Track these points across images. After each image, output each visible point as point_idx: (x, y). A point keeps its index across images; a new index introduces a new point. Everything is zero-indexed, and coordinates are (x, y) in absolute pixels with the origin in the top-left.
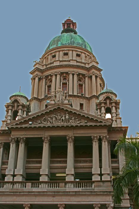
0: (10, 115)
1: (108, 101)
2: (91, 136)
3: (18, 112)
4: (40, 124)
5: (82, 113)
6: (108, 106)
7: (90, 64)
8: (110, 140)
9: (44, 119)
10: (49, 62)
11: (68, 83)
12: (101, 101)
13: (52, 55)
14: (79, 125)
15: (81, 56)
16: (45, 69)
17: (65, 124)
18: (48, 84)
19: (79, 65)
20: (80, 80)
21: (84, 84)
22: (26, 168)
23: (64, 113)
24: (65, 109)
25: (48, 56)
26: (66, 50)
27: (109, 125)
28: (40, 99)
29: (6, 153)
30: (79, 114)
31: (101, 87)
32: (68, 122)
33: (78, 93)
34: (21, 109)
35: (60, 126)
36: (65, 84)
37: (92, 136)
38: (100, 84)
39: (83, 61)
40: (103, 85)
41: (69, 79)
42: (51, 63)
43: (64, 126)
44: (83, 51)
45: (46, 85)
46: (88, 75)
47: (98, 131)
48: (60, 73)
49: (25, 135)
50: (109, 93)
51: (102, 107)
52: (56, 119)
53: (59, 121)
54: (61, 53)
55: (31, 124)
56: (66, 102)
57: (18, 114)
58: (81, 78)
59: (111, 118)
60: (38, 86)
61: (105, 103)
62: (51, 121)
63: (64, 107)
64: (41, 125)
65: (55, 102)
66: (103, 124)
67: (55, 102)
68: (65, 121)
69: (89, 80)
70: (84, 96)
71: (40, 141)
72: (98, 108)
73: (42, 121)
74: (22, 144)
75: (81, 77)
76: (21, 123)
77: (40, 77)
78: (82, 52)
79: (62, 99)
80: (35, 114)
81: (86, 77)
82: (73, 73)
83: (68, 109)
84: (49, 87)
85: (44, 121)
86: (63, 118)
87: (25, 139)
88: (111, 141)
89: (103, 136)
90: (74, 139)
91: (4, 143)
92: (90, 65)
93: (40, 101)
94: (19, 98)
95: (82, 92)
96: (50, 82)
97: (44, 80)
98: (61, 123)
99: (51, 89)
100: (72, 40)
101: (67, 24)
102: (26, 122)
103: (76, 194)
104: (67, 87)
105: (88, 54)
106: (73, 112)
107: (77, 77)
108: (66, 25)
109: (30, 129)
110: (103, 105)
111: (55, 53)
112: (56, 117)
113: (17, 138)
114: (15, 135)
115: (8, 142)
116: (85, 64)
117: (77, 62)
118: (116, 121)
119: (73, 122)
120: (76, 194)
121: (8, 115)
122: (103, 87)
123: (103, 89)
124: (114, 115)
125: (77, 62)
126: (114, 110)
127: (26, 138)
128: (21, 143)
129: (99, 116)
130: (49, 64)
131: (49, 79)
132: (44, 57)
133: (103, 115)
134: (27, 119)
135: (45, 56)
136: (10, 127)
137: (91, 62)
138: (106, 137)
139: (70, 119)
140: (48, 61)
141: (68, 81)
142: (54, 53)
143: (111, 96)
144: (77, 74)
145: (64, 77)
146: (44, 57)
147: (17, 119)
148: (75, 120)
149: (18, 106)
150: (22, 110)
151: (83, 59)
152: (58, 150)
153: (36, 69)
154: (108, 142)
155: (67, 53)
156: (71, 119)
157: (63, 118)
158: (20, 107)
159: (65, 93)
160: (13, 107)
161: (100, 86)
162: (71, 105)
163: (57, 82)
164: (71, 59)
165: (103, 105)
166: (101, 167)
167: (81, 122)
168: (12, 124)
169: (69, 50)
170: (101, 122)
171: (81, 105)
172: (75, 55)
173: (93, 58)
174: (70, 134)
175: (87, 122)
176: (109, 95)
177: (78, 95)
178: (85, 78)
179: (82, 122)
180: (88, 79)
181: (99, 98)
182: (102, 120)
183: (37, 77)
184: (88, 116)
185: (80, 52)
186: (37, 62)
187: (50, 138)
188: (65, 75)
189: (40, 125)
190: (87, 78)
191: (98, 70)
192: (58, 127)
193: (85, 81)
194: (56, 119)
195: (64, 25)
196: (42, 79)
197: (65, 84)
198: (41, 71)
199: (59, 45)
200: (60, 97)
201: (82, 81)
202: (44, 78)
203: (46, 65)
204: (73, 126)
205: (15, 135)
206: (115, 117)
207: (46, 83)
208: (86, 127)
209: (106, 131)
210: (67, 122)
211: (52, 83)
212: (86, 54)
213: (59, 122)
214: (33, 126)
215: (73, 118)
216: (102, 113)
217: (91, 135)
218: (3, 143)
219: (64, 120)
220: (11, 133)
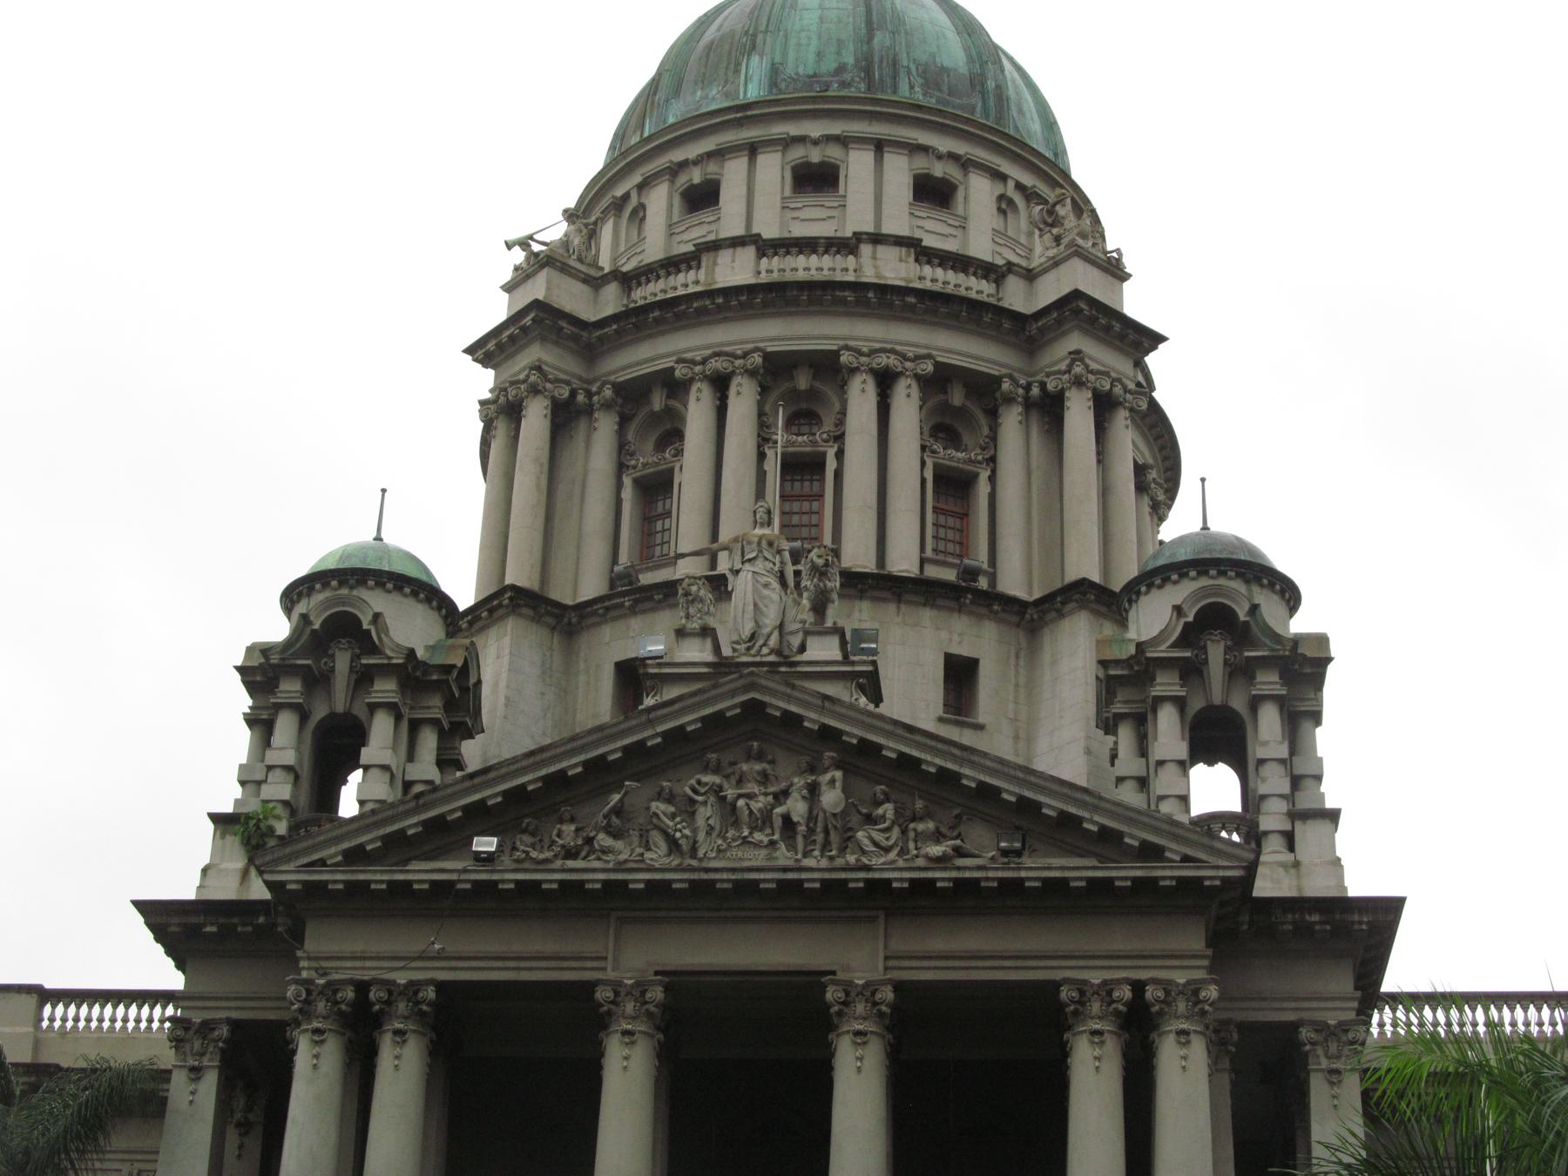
0: (289, 757)
1: (1216, 653)
2: (1056, 985)
3: (358, 735)
4: (571, 854)
5: (973, 765)
6: (1217, 699)
7: (1049, 278)
8: (1228, 1022)
9: (618, 811)
10: (654, 247)
11: (831, 453)
12: (1154, 642)
13: (682, 180)
15: (960, 194)
16: (615, 318)
17: (816, 866)
18: (646, 458)
19: (937, 287)
20: (942, 428)
21: (984, 475)
23: (804, 760)
24: (813, 718)
25: (641, 187)
26: (816, 142)
27: (1224, 879)
28: (564, 607)
29: (238, 1116)
30: (941, 769)
31: (1146, 500)
32: (843, 850)
33: (929, 553)
34: (392, 708)
35: (812, 880)
36: (803, 468)
37: (1067, 981)
38: (1140, 470)
39: (981, 247)
40: (1160, 470)
41: (841, 422)
42: (672, 265)
43: (800, 882)
44: (981, 154)
45: (621, 468)
46: (1028, 388)
47: (1119, 937)
48: (757, 359)
49: (439, 956)
50: (1222, 573)
51: (1159, 701)
52: (729, 811)
53: (758, 836)
54: (772, 170)
55: (488, 859)
56: (824, 650)
57: (366, 755)
58: (961, 412)
59: (1237, 807)
60: (612, 515)
61: (1191, 671)
62: (682, 833)
63: (800, 702)
64: (579, 864)
65: (717, 648)
66: (1167, 873)
67: (717, 648)
68: (811, 831)
70: (983, 583)
71: (576, 1018)
72: (1119, 708)
73: (598, 829)
74: (197, 1079)
75: (960, 409)
76: (398, 847)
77: (565, 393)
78: (966, 164)
79: (781, 626)
80: (535, 756)
81: (1009, 400)
82: (883, 360)
83: (841, 717)
85: (616, 835)
86: (797, 807)
87: (431, 993)
88: (1243, 1027)
89: (1166, 985)
90: (894, 1007)
91: (235, 1025)
92: (1050, 290)
93: (563, 621)
94: (375, 601)
95: (965, 545)
96: (661, 445)
97: (605, 426)
98: (770, 858)
99: (668, 514)
102: (444, 835)
104: (820, 513)
105: (1028, 180)
106: (892, 747)
107: (924, 400)
109: (484, 901)
110: (1166, 684)
111: (712, 168)
112: (730, 793)
113: (362, 987)
114: (342, 952)
115: (272, 1016)
116: (992, 272)
117: (925, 255)
118: (1290, 839)
119: (887, 850)
121: (272, 757)
122: (1161, 497)
123: (1159, 511)
124: (1273, 782)
125: (925, 255)
126: (1268, 726)
127: (441, 986)
128: (397, 1032)
129: (1129, 795)
130: (647, 273)
131: (653, 414)
132: (605, 202)
133: (1164, 782)
134: (452, 809)
135: (619, 192)
136: (291, 875)
137: (1056, 263)
138: (1196, 992)
139: (855, 819)
140: (642, 240)
141: (840, 438)
142: (696, 162)
143: (1239, 596)
144: (917, 377)
145: (793, 395)
146: (601, 203)
147: (348, 805)
148: (904, 832)
149: (363, 678)
150: (398, 718)
151: (978, 225)
153: (527, 321)
154: (1217, 1046)
155: (822, 164)
156: (870, 820)
157: (797, 807)
158: (385, 689)
159: (814, 568)
160: (316, 681)
161: (1141, 488)
162: (871, 685)
163: (722, 463)
164: (870, 228)
165: (1166, 684)
167: (959, 852)
168: (306, 852)
169: (843, 141)
170: (1150, 852)
171: (960, 675)
172: (908, 194)
173: (1070, 221)
174: (858, 960)
175: (1019, 853)
176: (1218, 590)
177: (933, 572)
178: (993, 414)
179: (968, 846)
181: (1132, 615)
182: (1156, 831)
183: (535, 391)
184: (988, 779)
185: (953, 157)
186: (536, 247)
187: (667, 989)
188: (803, 381)
189: (570, 864)
190: (1011, 422)
191: (1122, 337)
192: (746, 890)
193: (994, 438)
194: (729, 811)
196: (589, 411)
197: (803, 468)
198: (575, 338)
199: (753, 91)
200: (755, 605)
201: (967, 439)
202: (607, 406)
203: (628, 280)
204: (888, 881)
206: (1281, 806)
207: (623, 450)
208: (1055, 899)
209: (1192, 938)
210: (826, 845)
211: (679, 453)
212: (1003, 178)
213: (757, 845)
214: (508, 877)
215: (888, 810)
216: (1160, 763)
217: (1058, 975)
218: (224, 1031)
219: (802, 828)
220: (298, 936)
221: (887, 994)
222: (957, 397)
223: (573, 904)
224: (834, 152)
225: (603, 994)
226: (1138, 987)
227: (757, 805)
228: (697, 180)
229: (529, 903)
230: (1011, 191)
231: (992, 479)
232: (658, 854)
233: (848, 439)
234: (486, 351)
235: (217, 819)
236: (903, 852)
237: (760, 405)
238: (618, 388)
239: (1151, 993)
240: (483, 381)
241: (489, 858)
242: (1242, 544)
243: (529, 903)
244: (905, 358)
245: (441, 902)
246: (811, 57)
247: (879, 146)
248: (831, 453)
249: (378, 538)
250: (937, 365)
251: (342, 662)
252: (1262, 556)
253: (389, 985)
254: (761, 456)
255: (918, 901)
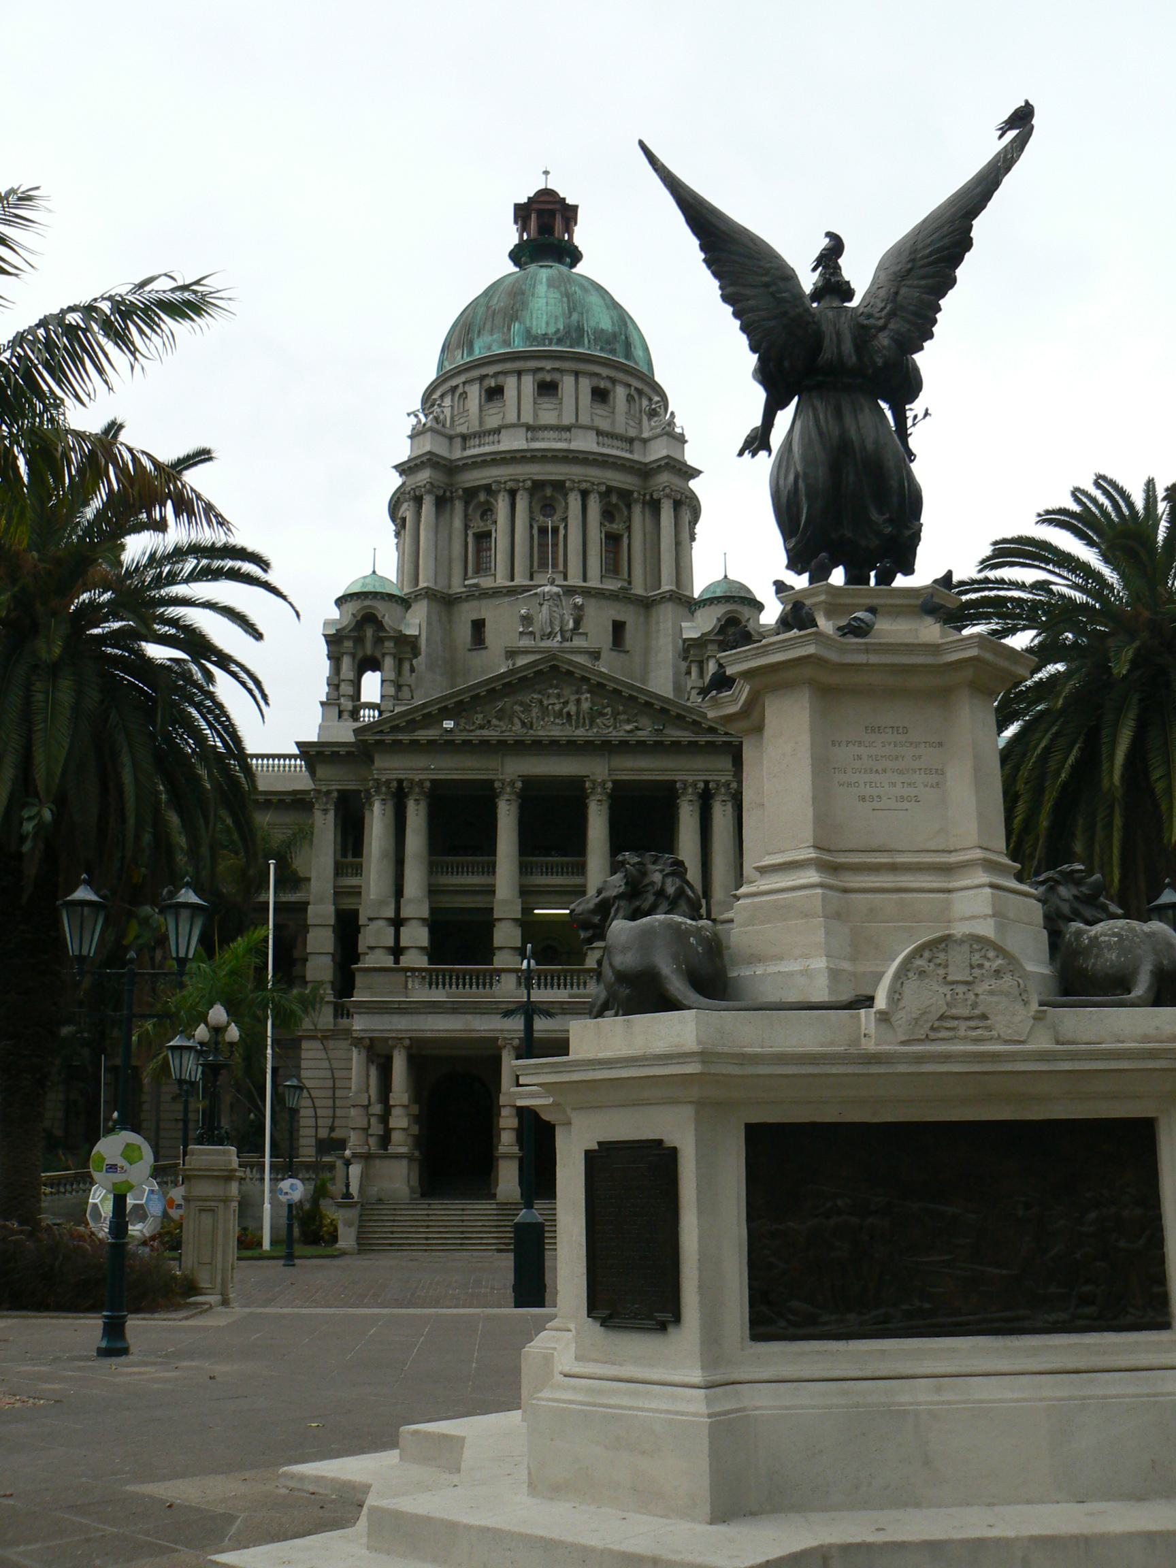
2: (675, 782)
4: (481, 727)
14: (632, 739)
18: (478, 525)
20: (608, 514)
21: (626, 535)
22: (433, 891)
25: (464, 383)
32: (591, 726)
46: (644, 495)
47: (699, 762)
48: (529, 483)
52: (544, 710)
53: (557, 721)
58: (616, 505)
69: (647, 520)
75: (616, 504)
78: (613, 381)
81: (637, 501)
84: (483, 537)
85: (500, 719)
89: (717, 783)
97: (459, 506)
100: (575, 316)
101: (540, 213)
103: (433, 1008)
108: (533, 216)
109: (447, 746)
113: (400, 782)
114: (390, 767)
120: (433, 1008)
127: (432, 781)
143: (746, 612)
149: (379, 641)
152: (552, 824)
156: (602, 714)
157: (572, 708)
158: (389, 645)
160: (359, 641)
163: (510, 526)
166: (399, 892)
167: (637, 728)
171: (618, 628)
174: (597, 770)
178: (629, 507)
180: (643, 512)
185: (608, 378)
190: (637, 510)
193: (629, 519)
194: (544, 710)
195: (522, 213)
196: (452, 499)
205: (390, 767)
208: (676, 747)
210: (584, 725)
212: (630, 386)
214: (459, 737)
215: (608, 710)
217: (677, 778)
221: (609, 785)
222: (614, 499)
223: (485, 747)
224: (557, 376)
225: (497, 785)
226: (707, 783)
227: (557, 707)
228: (493, 385)
229: (467, 747)
230: (633, 392)
231: (629, 537)
232: (517, 727)
233: (569, 520)
234: (403, 469)
235: (322, 704)
236: (615, 728)
237: (530, 503)
238: (465, 490)
239: (711, 785)
240: (396, 481)
241: (451, 730)
242: (743, 587)
243: (467, 747)
244: (593, 484)
245: (431, 747)
246: (544, 325)
247: (577, 374)
248: (562, 527)
249: (374, 572)
250: (607, 486)
251: (369, 632)
252: (749, 591)
253: (411, 781)
254: (531, 527)
255: (624, 747)
